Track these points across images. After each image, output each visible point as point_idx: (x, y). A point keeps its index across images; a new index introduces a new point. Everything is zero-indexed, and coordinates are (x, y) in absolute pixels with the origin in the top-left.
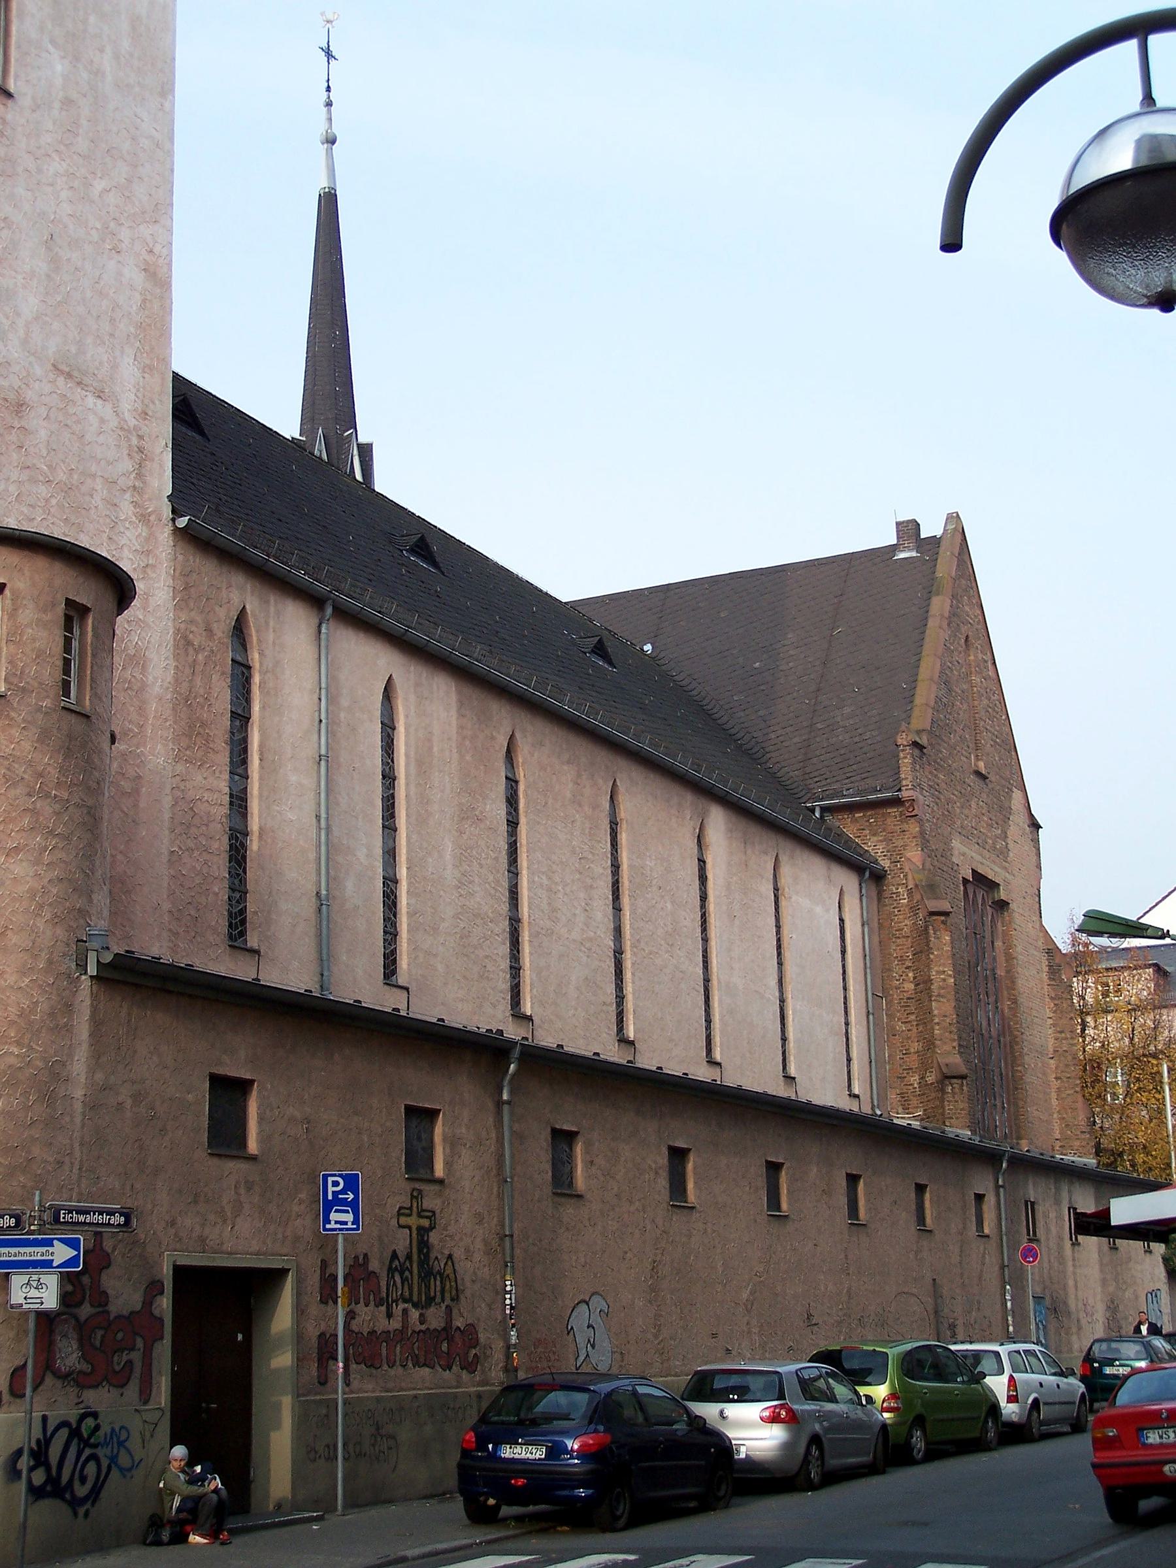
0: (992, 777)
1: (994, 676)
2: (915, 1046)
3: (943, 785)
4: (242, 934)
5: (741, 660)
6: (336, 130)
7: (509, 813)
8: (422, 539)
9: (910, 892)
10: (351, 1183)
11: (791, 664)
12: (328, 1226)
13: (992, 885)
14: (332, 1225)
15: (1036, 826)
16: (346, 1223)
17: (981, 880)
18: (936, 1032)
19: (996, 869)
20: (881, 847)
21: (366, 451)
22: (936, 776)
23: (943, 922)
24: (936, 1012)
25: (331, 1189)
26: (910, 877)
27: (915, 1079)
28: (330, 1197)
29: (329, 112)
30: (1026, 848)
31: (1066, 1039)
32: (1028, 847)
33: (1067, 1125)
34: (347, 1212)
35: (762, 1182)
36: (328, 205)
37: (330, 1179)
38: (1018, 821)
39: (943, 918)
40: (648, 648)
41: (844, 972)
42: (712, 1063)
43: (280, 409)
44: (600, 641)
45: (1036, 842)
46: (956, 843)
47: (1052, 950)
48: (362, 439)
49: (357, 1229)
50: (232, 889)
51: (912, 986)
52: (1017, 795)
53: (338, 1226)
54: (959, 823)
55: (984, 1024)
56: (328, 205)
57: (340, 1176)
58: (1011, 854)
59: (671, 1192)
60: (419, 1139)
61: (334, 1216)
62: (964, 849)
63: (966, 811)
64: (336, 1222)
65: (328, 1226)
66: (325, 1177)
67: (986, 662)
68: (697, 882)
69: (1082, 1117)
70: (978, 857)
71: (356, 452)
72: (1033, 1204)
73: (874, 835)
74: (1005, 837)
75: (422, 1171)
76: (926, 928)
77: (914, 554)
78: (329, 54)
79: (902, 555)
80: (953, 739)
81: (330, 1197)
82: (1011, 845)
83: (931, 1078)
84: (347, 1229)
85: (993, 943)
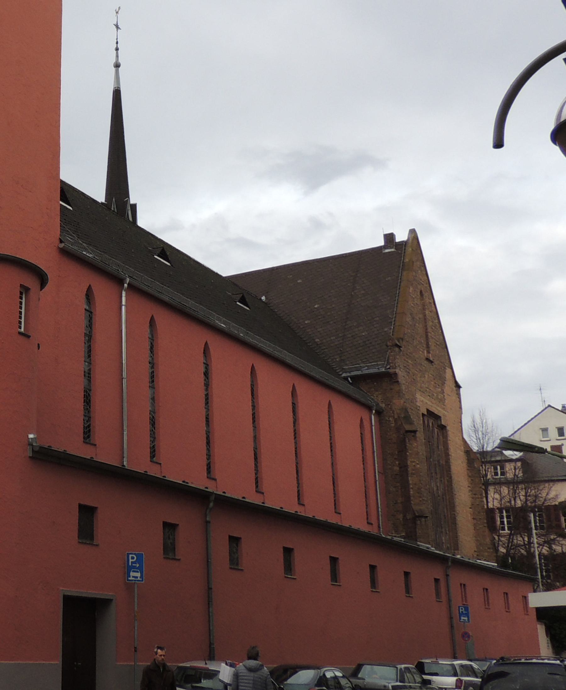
0: (436, 362)
1: (435, 310)
2: (400, 500)
3: (411, 366)
4: (89, 437)
5: (308, 304)
6: (120, 61)
7: (205, 380)
8: (163, 250)
9: (396, 420)
10: (140, 557)
11: (333, 306)
12: (129, 579)
13: (437, 417)
14: (131, 578)
15: (458, 386)
16: (137, 577)
17: (430, 414)
18: (411, 492)
19: (438, 408)
20: (380, 398)
21: (134, 207)
22: (408, 362)
23: (413, 436)
24: (411, 482)
25: (130, 560)
26: (395, 412)
27: (401, 517)
28: (130, 564)
29: (117, 53)
30: (454, 398)
31: (478, 498)
32: (454, 397)
33: (480, 544)
34: (138, 572)
35: (328, 567)
36: (117, 94)
37: (130, 556)
38: (449, 384)
39: (413, 434)
40: (263, 298)
41: (89, 337)
42: (301, 504)
43: (96, 189)
44: (243, 296)
45: (459, 395)
46: (418, 396)
47: (468, 451)
48: (132, 201)
49: (142, 581)
50: (85, 416)
51: (398, 469)
52: (448, 370)
53: (134, 579)
54: (419, 385)
55: (435, 489)
56: (117, 94)
57: (135, 554)
58: (446, 401)
59: (285, 571)
60: (169, 538)
61: (132, 574)
62: (422, 398)
63: (423, 379)
64: (133, 577)
65: (129, 579)
66: (128, 554)
67: (431, 303)
68: (292, 414)
69: (488, 540)
70: (429, 403)
71: (129, 208)
72: (464, 585)
73: (377, 391)
74: (443, 392)
75: (170, 554)
76: (405, 438)
77: (393, 250)
78: (117, 27)
79: (387, 251)
80: (415, 342)
81: (130, 564)
82: (446, 397)
83: (409, 516)
84: (138, 581)
85: (438, 447)
